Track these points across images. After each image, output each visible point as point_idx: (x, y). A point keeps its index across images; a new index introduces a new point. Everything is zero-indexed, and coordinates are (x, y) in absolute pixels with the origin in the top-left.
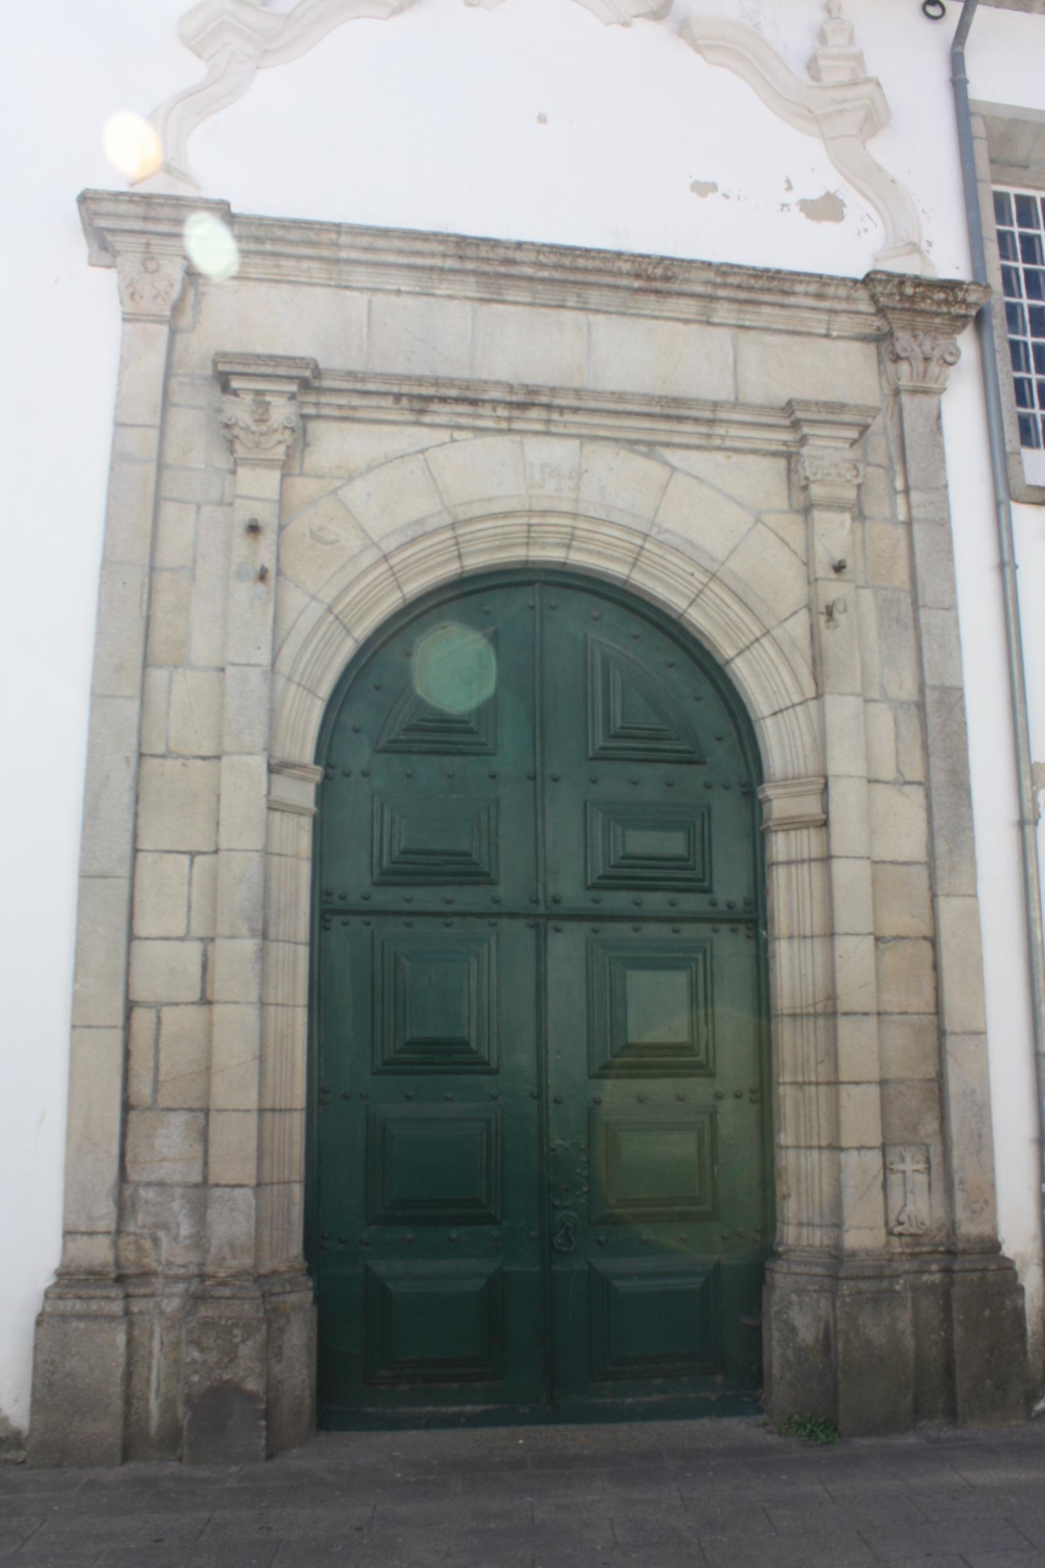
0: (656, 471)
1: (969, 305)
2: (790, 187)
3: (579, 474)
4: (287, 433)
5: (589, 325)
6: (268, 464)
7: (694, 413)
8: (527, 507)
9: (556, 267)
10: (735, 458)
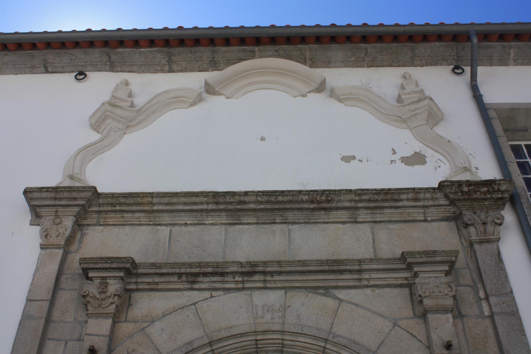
0: (329, 302)
1: (503, 192)
2: (394, 152)
3: (284, 308)
4: (116, 298)
5: (289, 230)
6: (105, 316)
7: (348, 267)
8: (253, 330)
9: (267, 202)
10: (377, 291)
